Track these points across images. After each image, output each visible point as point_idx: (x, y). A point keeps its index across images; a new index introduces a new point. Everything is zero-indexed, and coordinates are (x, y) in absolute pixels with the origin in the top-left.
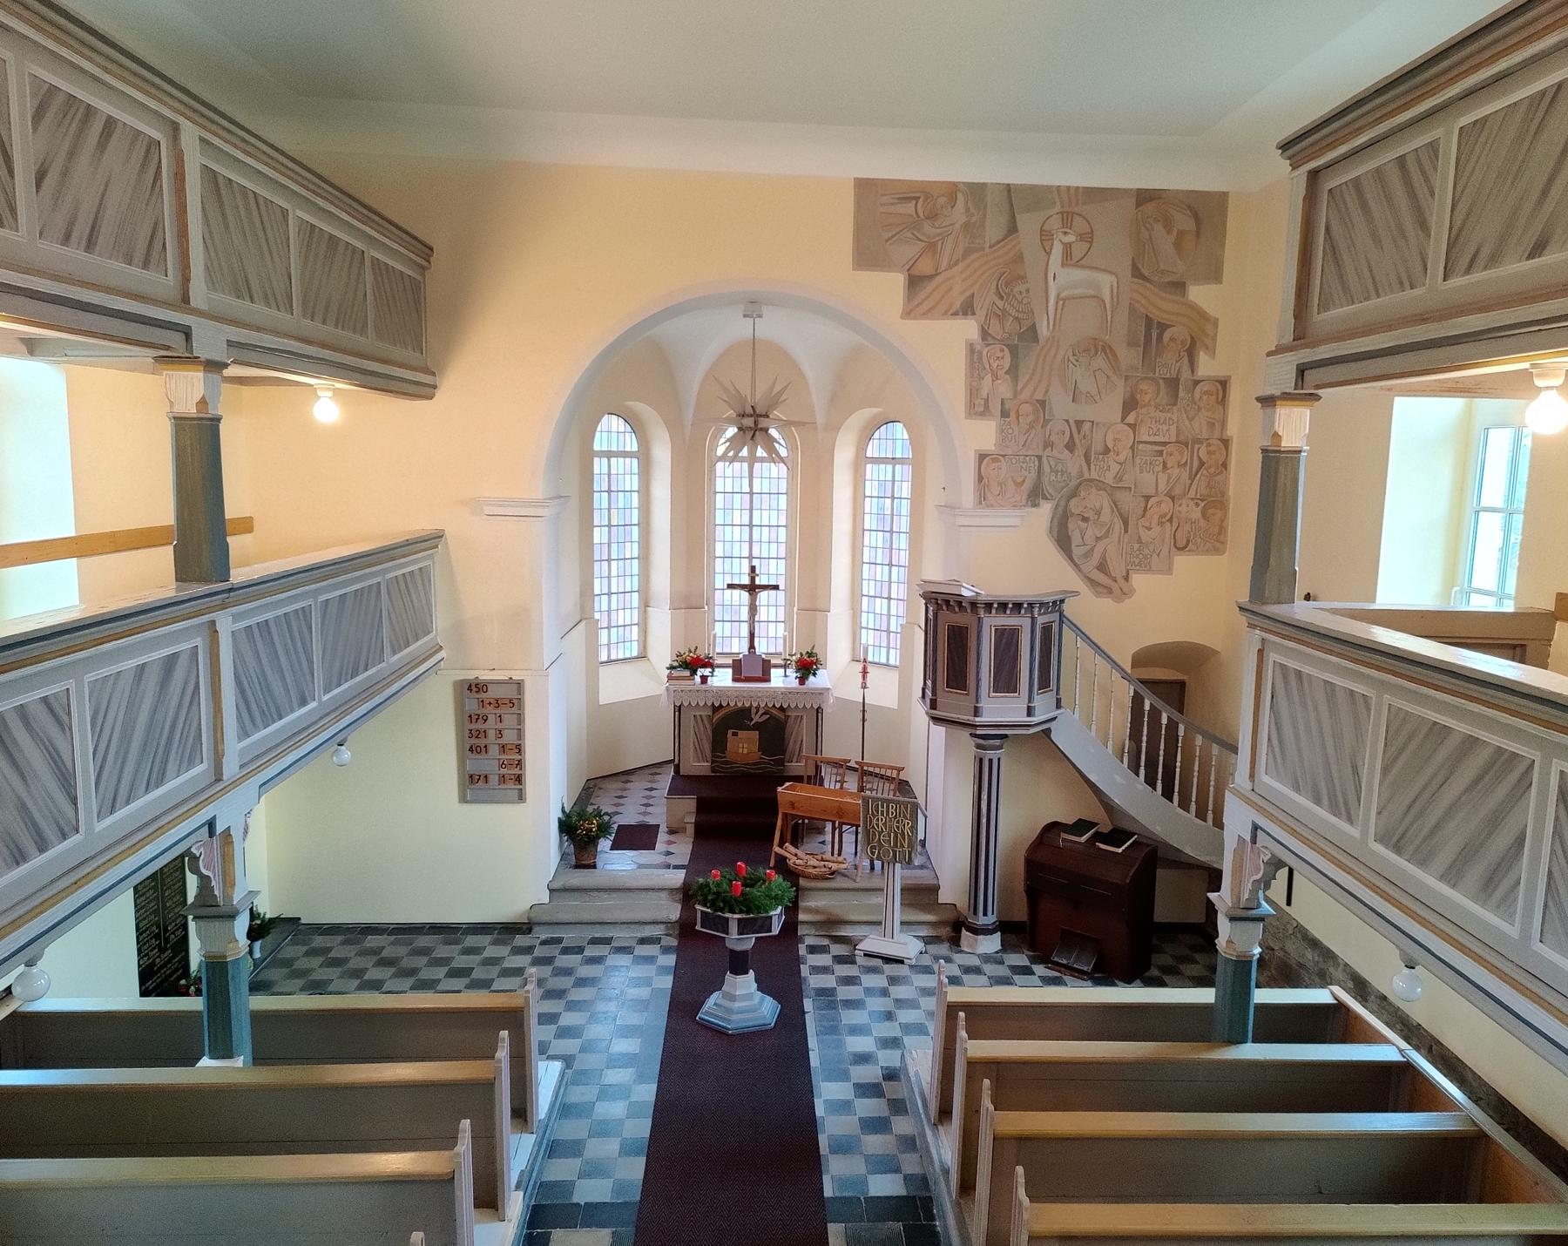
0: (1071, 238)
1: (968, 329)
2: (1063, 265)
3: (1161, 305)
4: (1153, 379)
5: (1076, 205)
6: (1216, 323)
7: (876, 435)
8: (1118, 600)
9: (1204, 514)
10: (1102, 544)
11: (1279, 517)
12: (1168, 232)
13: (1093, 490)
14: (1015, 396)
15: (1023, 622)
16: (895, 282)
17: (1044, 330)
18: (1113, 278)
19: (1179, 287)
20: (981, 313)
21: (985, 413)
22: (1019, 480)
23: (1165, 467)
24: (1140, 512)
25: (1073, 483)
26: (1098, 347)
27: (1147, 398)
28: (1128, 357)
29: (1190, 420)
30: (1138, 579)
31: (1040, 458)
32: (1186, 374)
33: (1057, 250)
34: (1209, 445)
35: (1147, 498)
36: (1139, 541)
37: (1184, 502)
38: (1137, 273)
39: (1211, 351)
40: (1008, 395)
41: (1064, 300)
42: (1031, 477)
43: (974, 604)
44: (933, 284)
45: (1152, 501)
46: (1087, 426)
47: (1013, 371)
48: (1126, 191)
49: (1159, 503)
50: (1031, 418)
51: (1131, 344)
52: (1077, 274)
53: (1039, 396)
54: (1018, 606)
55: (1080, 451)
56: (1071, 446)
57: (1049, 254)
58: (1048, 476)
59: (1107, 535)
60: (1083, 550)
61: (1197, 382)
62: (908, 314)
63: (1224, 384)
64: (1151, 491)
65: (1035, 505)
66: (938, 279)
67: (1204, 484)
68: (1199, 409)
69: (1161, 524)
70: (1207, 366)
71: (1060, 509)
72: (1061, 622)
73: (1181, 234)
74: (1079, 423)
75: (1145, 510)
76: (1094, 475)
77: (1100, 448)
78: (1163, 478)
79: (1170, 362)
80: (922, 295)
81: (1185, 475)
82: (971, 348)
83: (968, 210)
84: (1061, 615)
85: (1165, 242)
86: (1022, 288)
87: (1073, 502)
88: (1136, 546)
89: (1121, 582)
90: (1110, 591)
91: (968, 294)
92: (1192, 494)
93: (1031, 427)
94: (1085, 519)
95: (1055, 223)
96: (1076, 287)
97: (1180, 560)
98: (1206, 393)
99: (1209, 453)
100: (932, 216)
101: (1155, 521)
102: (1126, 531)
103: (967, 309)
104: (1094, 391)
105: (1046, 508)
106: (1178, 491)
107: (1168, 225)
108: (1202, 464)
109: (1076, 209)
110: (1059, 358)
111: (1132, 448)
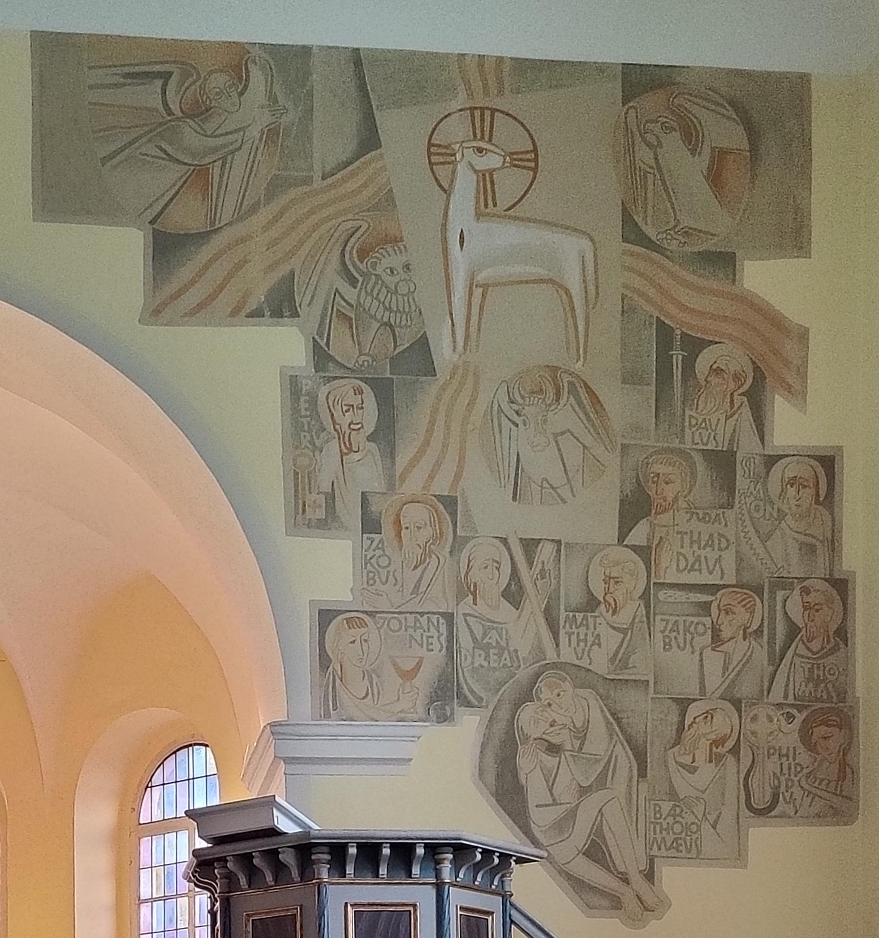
0: (493, 161)
1: (286, 345)
2: (479, 215)
3: (692, 301)
4: (681, 453)
5: (497, 96)
6: (803, 336)
7: (157, 779)
8: (635, 921)
9: (805, 735)
10: (596, 799)
11: (837, 489)
12: (693, 152)
13: (568, 686)
14: (391, 486)
15: (418, 895)
16: (123, 248)
17: (444, 352)
18: (586, 244)
19: (724, 262)
20: (311, 314)
21: (328, 522)
22: (409, 665)
23: (717, 639)
24: (670, 732)
25: (523, 674)
26: (556, 384)
27: (670, 492)
28: (626, 406)
29: (764, 539)
30: (670, 875)
31: (449, 618)
32: (748, 446)
33: (465, 186)
34: (806, 591)
35: (683, 704)
36: (673, 794)
37: (761, 712)
38: (632, 232)
39: (797, 393)
40: (377, 484)
41: (485, 287)
42: (433, 660)
43: (305, 848)
44: (205, 253)
45: (694, 710)
46: (546, 552)
47: (385, 434)
48: (601, 69)
49: (708, 715)
50: (427, 533)
51: (631, 378)
52: (507, 235)
53: (441, 487)
54: (403, 852)
55: (534, 604)
56: (514, 594)
57: (447, 192)
58: (469, 659)
59: (601, 782)
60: (552, 815)
61: (771, 461)
62: (155, 313)
63: (828, 462)
64: (693, 690)
65: (444, 718)
66: (219, 241)
67: (800, 676)
68: (781, 516)
69: (715, 759)
70: (791, 427)
71: (500, 727)
72: (508, 922)
73: (720, 156)
74: (530, 545)
75: (681, 729)
76: (567, 655)
77: (577, 597)
78: (714, 662)
79: (714, 420)
80: (186, 273)
81: (761, 655)
82: (293, 386)
83: (273, 99)
84: (505, 897)
85: (688, 170)
86: (396, 261)
87: (527, 713)
88: (666, 807)
89: (638, 881)
90: (616, 903)
91: (283, 270)
92: (777, 694)
93: (427, 553)
94: (554, 749)
95: (456, 130)
96: (509, 271)
97: (762, 837)
98: (792, 482)
99: (807, 607)
100: (199, 112)
101: (701, 756)
102: (642, 773)
103: (281, 305)
104: (556, 476)
105: (468, 727)
106: (746, 689)
107: (691, 137)
108: (793, 631)
109: (498, 103)
110: (482, 405)
111: (645, 596)
